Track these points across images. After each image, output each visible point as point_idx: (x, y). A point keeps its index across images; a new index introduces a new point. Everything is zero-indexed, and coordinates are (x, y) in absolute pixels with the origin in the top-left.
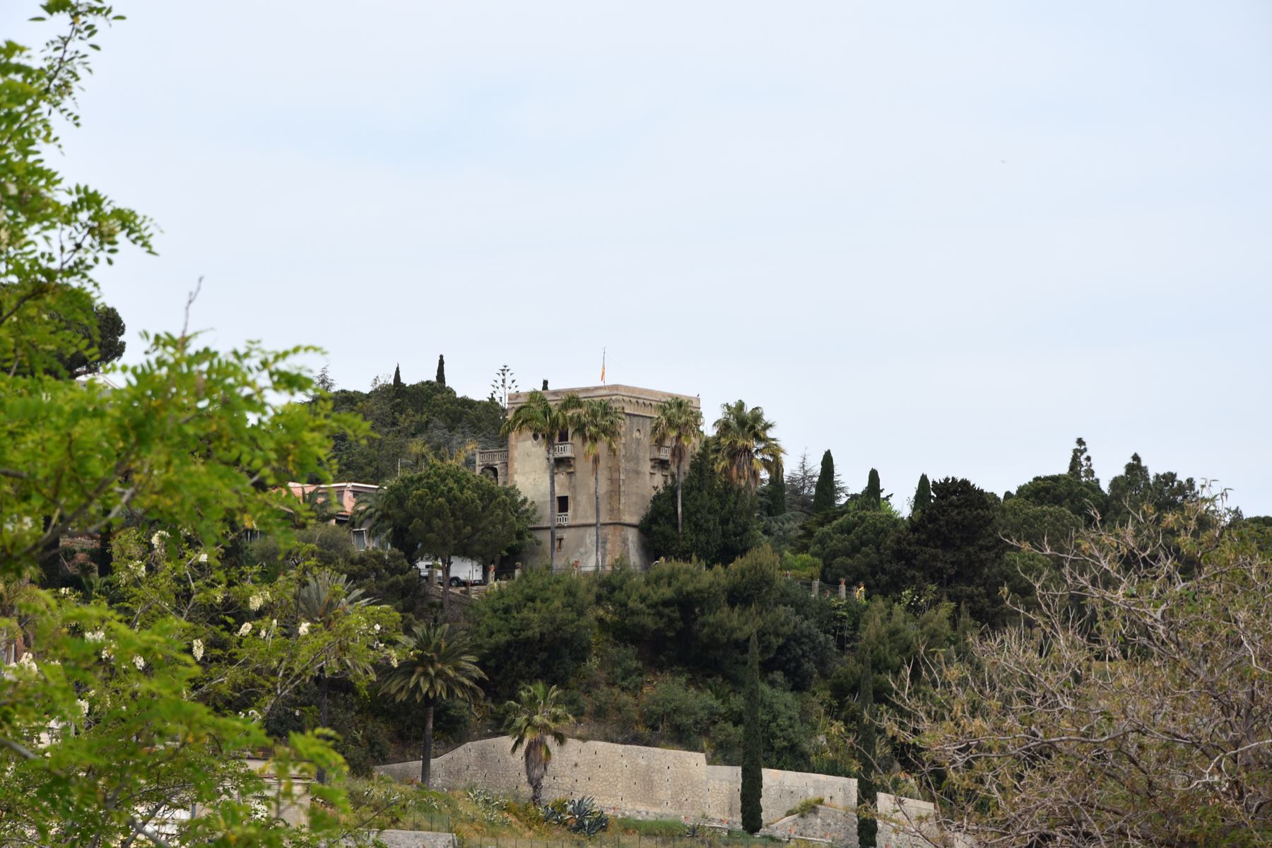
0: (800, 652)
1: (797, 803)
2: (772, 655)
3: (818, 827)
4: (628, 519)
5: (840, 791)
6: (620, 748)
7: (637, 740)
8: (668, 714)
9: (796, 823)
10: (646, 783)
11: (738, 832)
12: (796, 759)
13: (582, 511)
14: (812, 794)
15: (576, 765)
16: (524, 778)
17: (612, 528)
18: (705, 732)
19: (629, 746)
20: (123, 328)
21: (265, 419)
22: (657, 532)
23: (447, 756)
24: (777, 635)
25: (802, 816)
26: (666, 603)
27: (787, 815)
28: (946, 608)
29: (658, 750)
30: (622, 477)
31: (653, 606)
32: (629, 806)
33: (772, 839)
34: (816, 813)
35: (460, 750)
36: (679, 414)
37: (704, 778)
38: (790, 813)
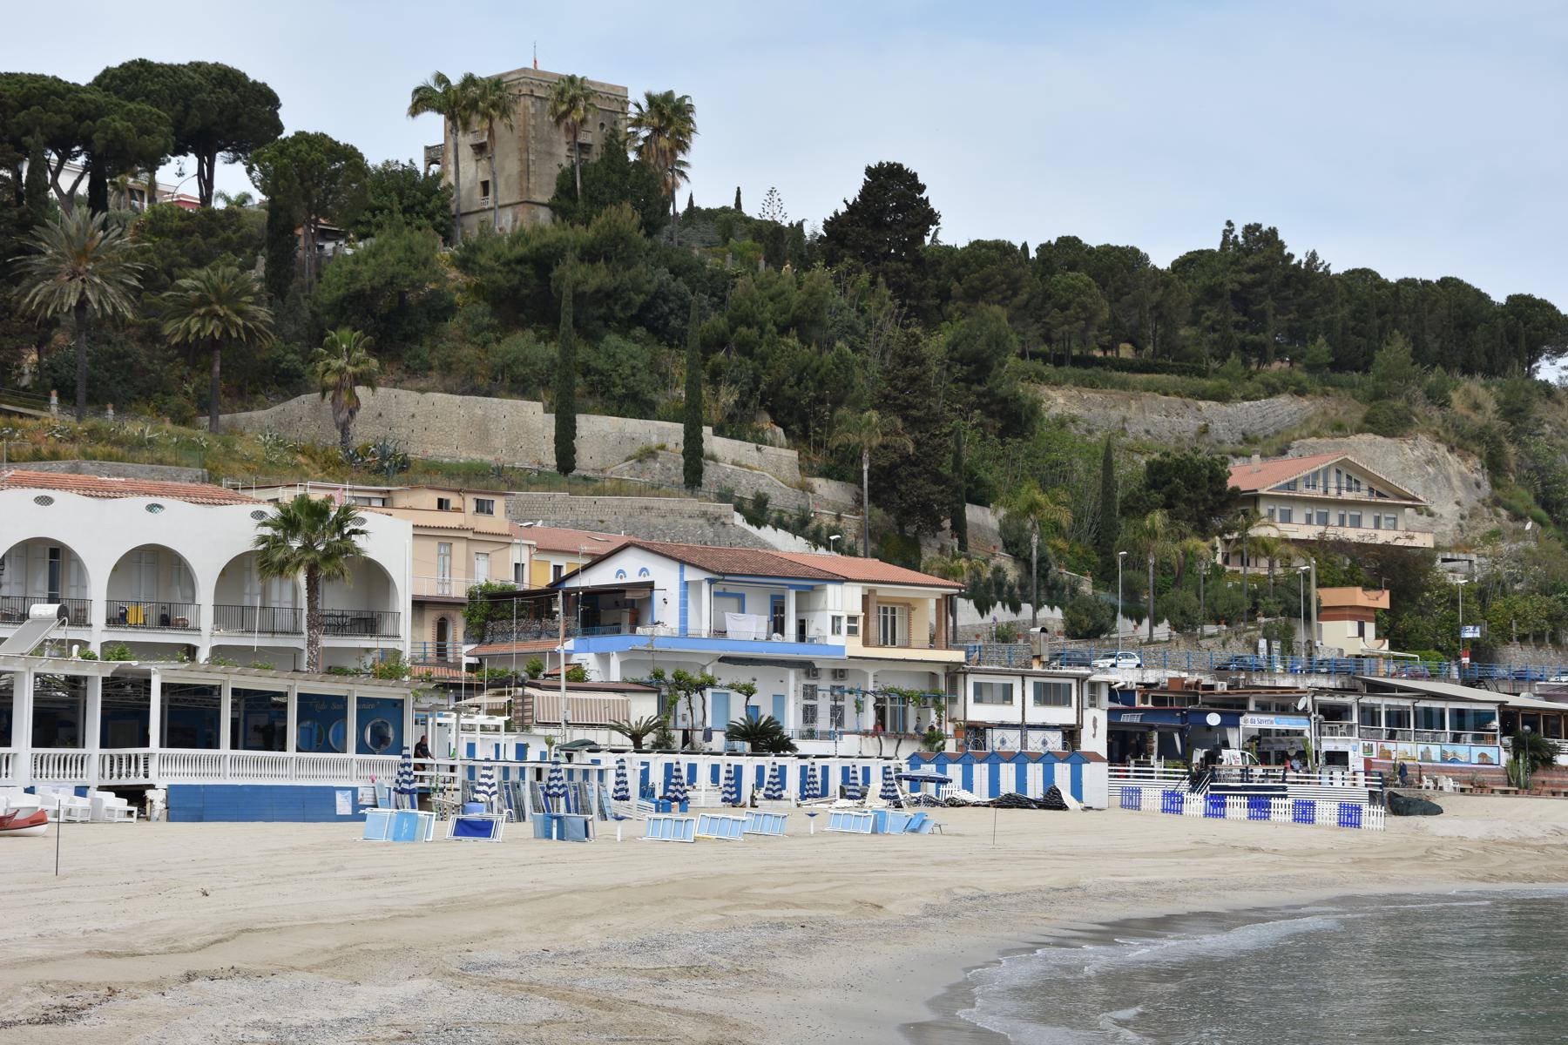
1: (630, 450)
4: (539, 198)
5: (672, 433)
6: (458, 399)
7: (475, 391)
9: (632, 468)
10: (482, 431)
11: (551, 474)
12: (636, 405)
14: (655, 441)
16: (613, 500)
18: (544, 384)
21: (673, 284)
22: (566, 200)
23: (278, 408)
24: (639, 291)
26: (520, 261)
28: (866, 276)
29: (496, 400)
30: (532, 157)
31: (507, 263)
35: (294, 402)
36: (570, 98)
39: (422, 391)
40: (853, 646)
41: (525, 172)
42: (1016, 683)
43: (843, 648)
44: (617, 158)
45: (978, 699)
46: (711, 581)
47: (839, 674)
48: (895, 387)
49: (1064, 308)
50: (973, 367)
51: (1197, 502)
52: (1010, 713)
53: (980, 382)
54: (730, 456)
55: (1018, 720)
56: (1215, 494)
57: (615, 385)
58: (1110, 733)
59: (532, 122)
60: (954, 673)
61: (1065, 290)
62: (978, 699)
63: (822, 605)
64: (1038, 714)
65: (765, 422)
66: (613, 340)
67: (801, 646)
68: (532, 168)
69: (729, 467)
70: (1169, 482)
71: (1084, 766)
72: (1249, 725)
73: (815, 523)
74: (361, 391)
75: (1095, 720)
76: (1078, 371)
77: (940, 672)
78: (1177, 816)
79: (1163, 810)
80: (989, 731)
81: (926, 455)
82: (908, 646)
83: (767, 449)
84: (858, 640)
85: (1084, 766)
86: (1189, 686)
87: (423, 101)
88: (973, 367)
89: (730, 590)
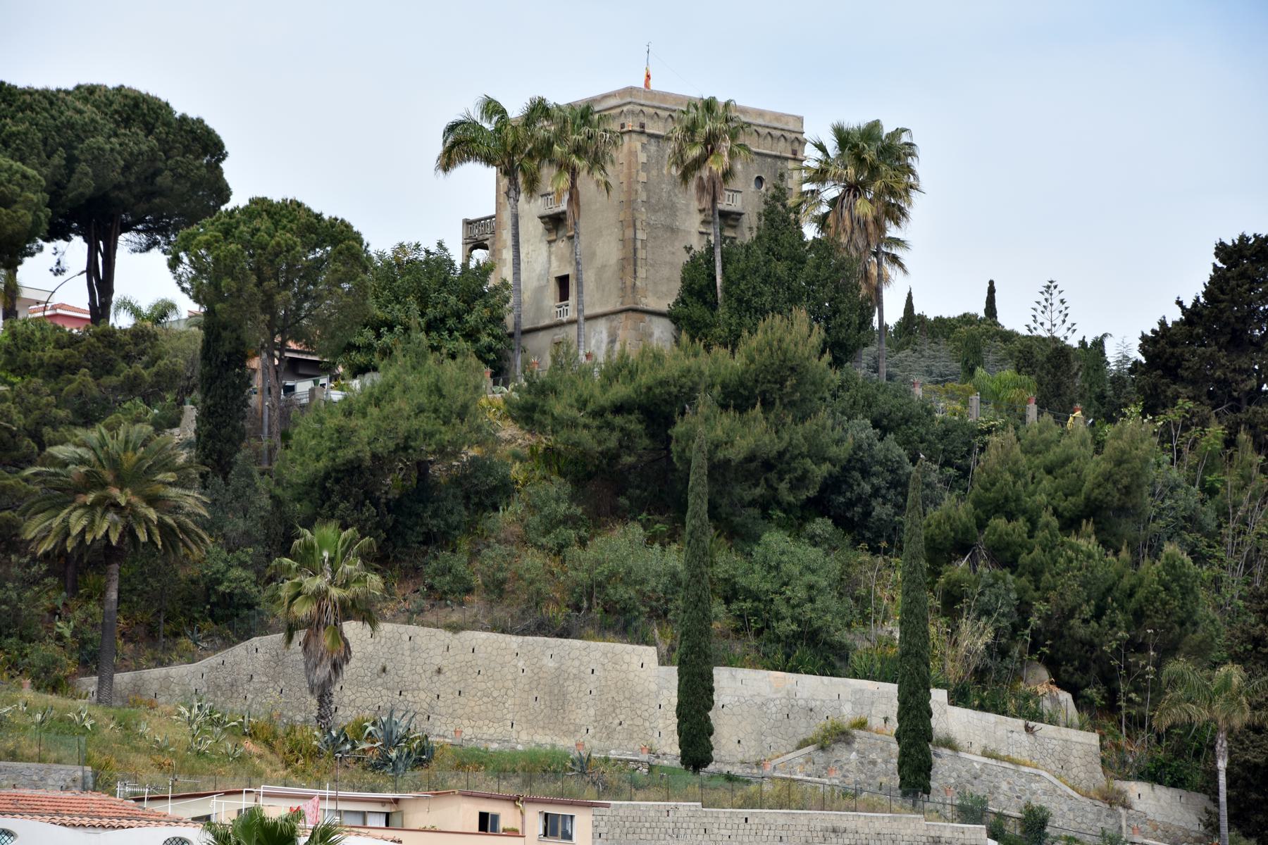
0: (868, 488)
1: (813, 728)
2: (812, 493)
3: (852, 767)
6: (514, 641)
7: (543, 628)
8: (600, 585)
10: (554, 697)
12: (817, 652)
13: (596, 294)
14: (848, 713)
15: (439, 671)
17: (623, 316)
19: (530, 638)
20: (451, 128)
22: (701, 304)
23: (214, 660)
24: (820, 458)
25: (823, 748)
27: (798, 748)
28: (1216, 431)
31: (599, 413)
32: (524, 737)
33: (730, 778)
34: (849, 743)
35: (240, 650)
36: (705, 135)
37: (653, 687)
38: (804, 744)
41: (630, 261)
44: (788, 246)
54: (979, 742)
57: (779, 617)
59: (643, 177)
65: (1039, 680)
68: (641, 254)
74: (352, 629)
83: (1044, 729)
87: (461, 144)
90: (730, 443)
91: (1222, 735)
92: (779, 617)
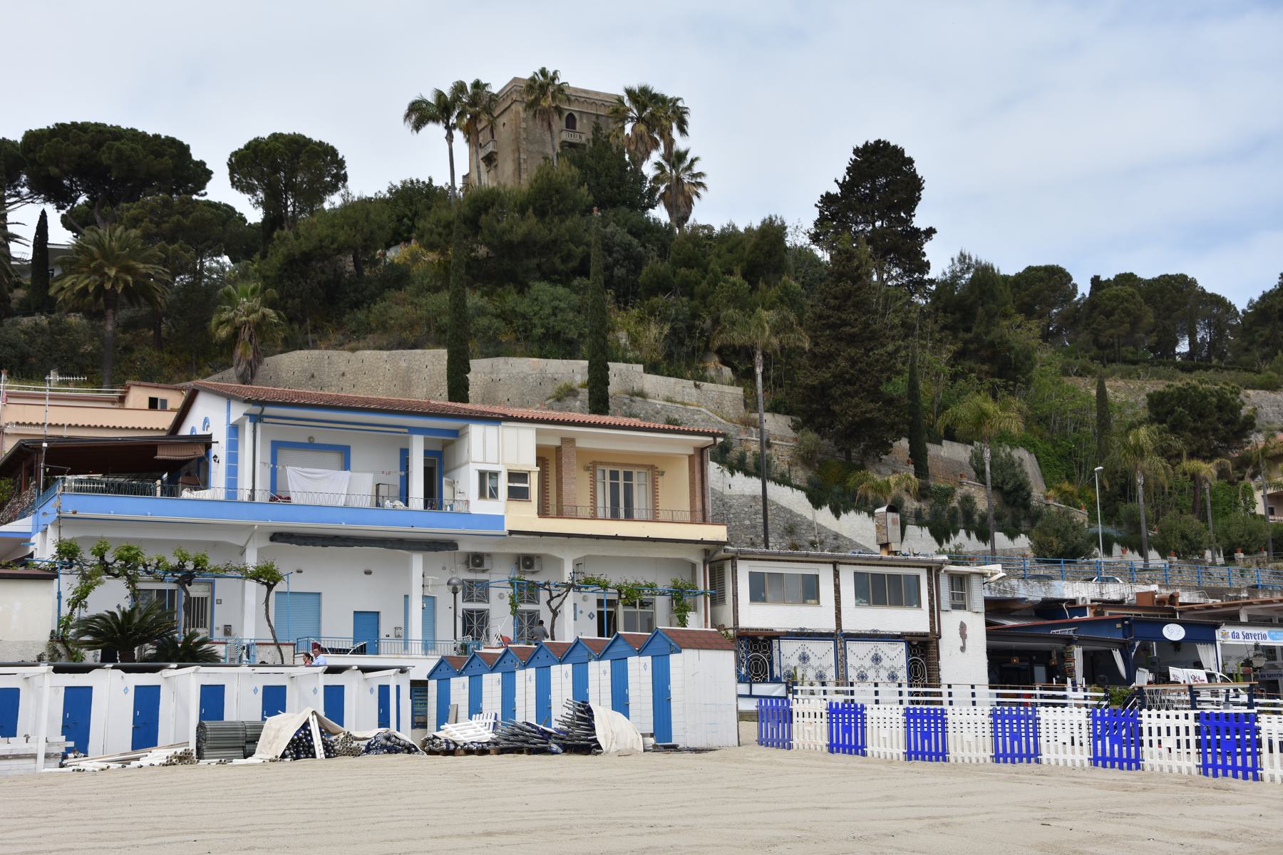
1: (550, 390)
6: (385, 354)
10: (406, 381)
39: (353, 350)
40: (524, 516)
42: (825, 575)
43: (500, 519)
45: (757, 595)
46: (256, 419)
47: (527, 562)
48: (828, 307)
49: (1108, 315)
50: (958, 316)
51: (1205, 431)
52: (818, 617)
53: (968, 330)
54: (665, 392)
55: (830, 626)
56: (1226, 423)
57: (535, 326)
58: (992, 653)
59: (523, 125)
60: (716, 561)
61: (1110, 300)
62: (757, 595)
63: (465, 459)
64: (860, 618)
65: (713, 364)
66: (540, 288)
67: (433, 515)
68: (523, 166)
69: (659, 403)
70: (1171, 412)
71: (673, 658)
72: (1230, 641)
73: (740, 449)
75: (963, 627)
76: (1125, 367)
77: (697, 559)
78: (854, 760)
79: (997, 758)
80: (775, 642)
81: (861, 371)
82: (655, 519)
83: (705, 385)
84: (531, 507)
85: (673, 657)
86: (1161, 601)
87: (420, 114)
88: (958, 316)
89: (321, 437)
90: (511, 230)
91: (759, 352)
92: (535, 326)
